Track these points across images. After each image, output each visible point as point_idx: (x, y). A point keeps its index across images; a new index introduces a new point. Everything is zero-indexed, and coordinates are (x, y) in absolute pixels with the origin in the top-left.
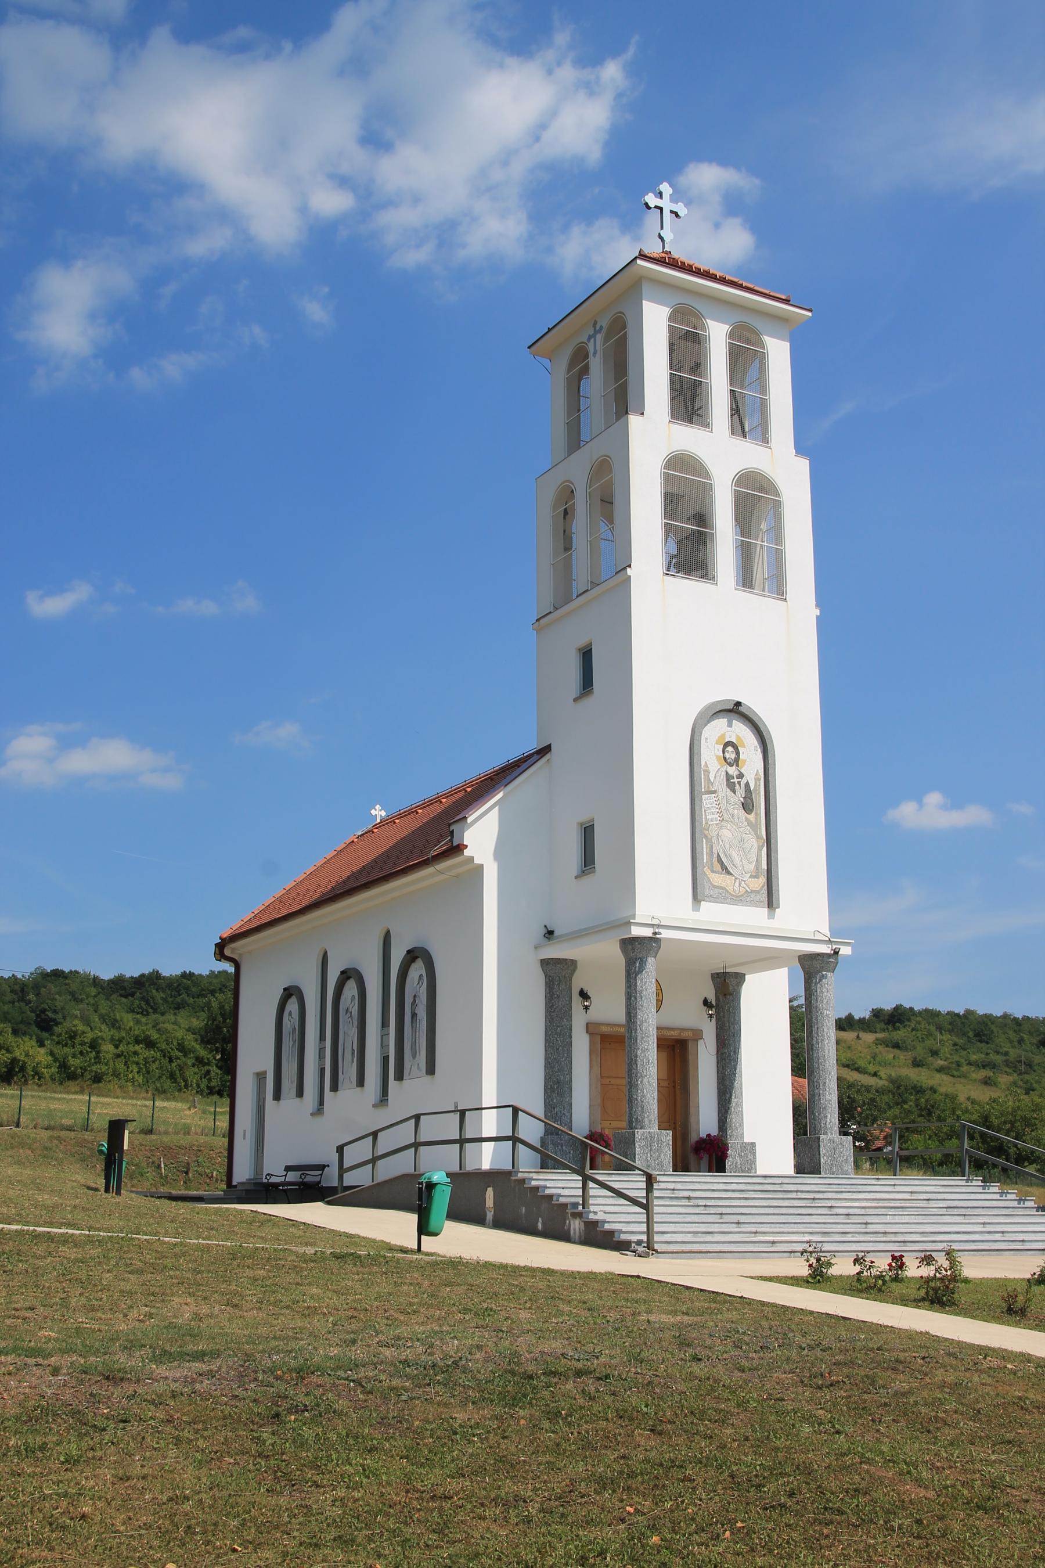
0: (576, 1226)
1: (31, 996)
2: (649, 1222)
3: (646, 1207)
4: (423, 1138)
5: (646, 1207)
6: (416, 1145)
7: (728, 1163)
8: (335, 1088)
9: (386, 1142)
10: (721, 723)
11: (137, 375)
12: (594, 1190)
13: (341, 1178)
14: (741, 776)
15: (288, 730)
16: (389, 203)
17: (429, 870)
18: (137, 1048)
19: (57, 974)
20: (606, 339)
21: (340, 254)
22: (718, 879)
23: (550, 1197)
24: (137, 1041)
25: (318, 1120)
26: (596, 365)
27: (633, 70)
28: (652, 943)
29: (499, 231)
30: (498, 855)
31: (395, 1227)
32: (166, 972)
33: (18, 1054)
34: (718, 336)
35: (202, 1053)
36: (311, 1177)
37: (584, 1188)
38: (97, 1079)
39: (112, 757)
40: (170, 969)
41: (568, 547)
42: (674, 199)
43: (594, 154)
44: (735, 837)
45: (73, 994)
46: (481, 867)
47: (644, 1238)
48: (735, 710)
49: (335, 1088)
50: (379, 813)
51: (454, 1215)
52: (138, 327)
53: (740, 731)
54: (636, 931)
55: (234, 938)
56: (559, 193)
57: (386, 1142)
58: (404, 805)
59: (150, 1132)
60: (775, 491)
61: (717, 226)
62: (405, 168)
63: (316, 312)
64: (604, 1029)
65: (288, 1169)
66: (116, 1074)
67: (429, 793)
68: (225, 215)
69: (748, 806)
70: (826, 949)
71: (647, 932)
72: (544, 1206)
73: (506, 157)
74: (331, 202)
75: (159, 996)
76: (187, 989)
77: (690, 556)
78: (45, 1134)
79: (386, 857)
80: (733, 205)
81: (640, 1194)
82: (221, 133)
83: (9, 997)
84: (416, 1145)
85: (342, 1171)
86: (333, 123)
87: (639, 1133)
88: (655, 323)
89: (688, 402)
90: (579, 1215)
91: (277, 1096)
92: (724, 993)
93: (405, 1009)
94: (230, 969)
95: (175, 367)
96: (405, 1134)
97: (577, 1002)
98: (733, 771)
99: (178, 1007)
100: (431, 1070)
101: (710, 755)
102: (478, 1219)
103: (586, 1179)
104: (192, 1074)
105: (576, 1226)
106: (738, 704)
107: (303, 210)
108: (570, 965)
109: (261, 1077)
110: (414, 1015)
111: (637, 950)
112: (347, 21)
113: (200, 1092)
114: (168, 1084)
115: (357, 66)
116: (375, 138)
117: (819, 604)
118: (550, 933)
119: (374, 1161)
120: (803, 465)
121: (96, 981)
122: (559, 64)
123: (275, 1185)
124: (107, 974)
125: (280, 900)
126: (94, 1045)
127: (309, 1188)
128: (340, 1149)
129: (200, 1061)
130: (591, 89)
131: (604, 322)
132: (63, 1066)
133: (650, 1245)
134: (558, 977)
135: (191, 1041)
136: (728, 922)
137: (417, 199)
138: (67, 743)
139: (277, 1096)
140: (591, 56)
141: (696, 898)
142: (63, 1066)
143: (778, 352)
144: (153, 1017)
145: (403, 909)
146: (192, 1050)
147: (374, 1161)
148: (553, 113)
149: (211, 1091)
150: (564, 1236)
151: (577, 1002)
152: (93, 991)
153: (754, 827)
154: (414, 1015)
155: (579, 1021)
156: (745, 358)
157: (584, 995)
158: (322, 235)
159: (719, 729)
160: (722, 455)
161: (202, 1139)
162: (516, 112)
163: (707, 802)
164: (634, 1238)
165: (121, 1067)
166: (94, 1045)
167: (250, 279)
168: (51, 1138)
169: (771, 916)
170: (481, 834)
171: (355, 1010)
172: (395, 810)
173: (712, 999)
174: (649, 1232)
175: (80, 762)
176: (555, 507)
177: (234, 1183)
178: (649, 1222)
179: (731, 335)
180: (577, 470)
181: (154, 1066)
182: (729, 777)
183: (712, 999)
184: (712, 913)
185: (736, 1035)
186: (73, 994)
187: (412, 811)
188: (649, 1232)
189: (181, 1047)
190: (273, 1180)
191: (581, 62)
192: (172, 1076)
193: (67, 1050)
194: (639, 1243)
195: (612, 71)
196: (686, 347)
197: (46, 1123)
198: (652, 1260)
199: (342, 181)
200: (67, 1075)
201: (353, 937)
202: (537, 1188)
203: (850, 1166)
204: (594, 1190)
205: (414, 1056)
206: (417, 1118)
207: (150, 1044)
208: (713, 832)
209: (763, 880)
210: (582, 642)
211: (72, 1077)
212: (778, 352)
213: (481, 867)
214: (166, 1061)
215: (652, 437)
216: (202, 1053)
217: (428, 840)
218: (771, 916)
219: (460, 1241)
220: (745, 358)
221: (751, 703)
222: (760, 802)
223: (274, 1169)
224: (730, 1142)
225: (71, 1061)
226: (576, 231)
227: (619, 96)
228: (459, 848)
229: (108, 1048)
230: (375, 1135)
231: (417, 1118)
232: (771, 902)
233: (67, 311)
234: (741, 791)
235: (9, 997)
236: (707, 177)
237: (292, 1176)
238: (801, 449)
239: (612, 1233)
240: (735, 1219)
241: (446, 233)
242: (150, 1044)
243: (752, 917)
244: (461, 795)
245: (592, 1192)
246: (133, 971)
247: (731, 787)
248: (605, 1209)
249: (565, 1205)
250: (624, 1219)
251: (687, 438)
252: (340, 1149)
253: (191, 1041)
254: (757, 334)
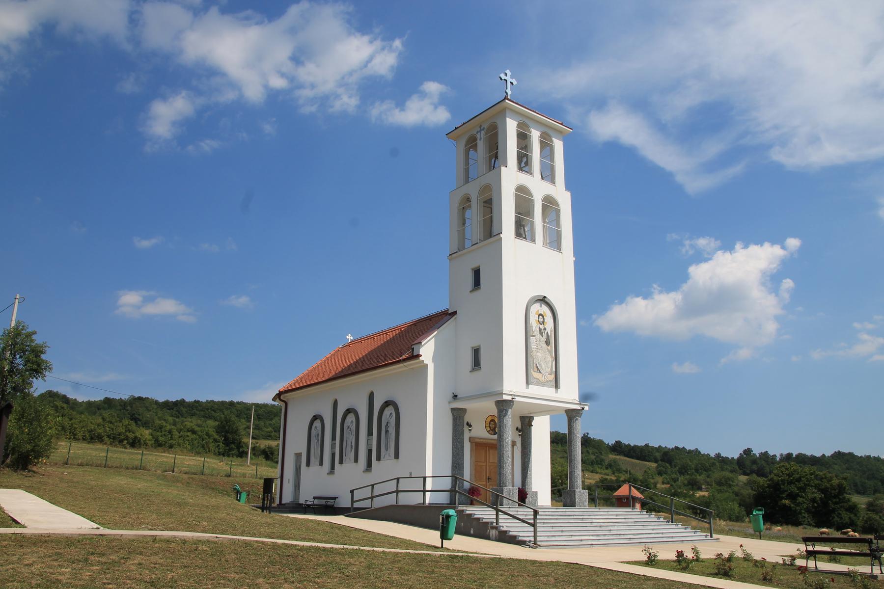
0: (493, 533)
1: (129, 408)
2: (535, 531)
3: (534, 525)
4: (400, 489)
5: (534, 525)
6: (397, 492)
7: (527, 500)
8: (341, 462)
9: (378, 490)
10: (538, 305)
11: (190, 148)
12: (501, 516)
13: (352, 504)
14: (545, 329)
15: (244, 300)
16: (301, 86)
17: (401, 365)
18: (189, 434)
19: (140, 398)
20: (486, 133)
21: (279, 104)
22: (536, 375)
23: (479, 519)
24: (188, 431)
25: (331, 476)
26: (481, 145)
27: (404, 44)
28: (510, 403)
29: (348, 102)
30: (434, 359)
31: (432, 537)
32: (187, 400)
33: (138, 434)
34: (535, 135)
35: (217, 437)
36: (330, 502)
37: (497, 515)
38: (171, 447)
39: (167, 306)
40: (189, 399)
41: (464, 224)
42: (512, 77)
43: (390, 77)
44: (543, 357)
45: (147, 408)
46: (427, 365)
47: (532, 539)
48: (543, 300)
49: (341, 462)
50: (350, 338)
51: (458, 532)
52: (192, 129)
53: (545, 309)
54: (505, 397)
55: (287, 391)
56: (371, 88)
57: (378, 490)
58: (364, 334)
59: (230, 476)
60: (558, 205)
61: (436, 107)
62: (309, 72)
63: (268, 128)
64: (477, 440)
65: (315, 498)
66: (179, 445)
67: (385, 327)
68: (234, 85)
69: (548, 343)
70: (578, 407)
71: (509, 398)
72: (474, 523)
73: (351, 73)
74: (278, 83)
75: (184, 410)
76: (196, 407)
77: (522, 230)
78: (186, 476)
79: (362, 360)
80: (443, 101)
81: (532, 521)
82: (234, 50)
83: (119, 408)
84: (397, 492)
85: (353, 502)
86: (282, 52)
87: (505, 489)
88: (511, 127)
89: (524, 162)
90: (496, 528)
91: (308, 464)
92: (525, 425)
93: (385, 428)
94: (283, 404)
95: (208, 145)
96: (392, 486)
97: (466, 428)
98: (542, 327)
99: (193, 415)
100: (397, 456)
101: (533, 319)
102: (468, 534)
103: (498, 511)
104: (212, 446)
105: (493, 533)
106: (545, 297)
107: (266, 86)
108: (464, 411)
109: (298, 456)
110: (387, 431)
111: (503, 406)
112: (294, 11)
113: (215, 454)
114: (201, 450)
115: (293, 31)
116: (297, 59)
117: (575, 255)
118: (456, 396)
119: (372, 498)
120: (568, 194)
121: (156, 402)
122: (375, 39)
123: (309, 506)
124: (161, 400)
125: (308, 375)
126: (170, 432)
127: (328, 507)
128: (352, 492)
129: (215, 440)
130: (391, 50)
131: (486, 126)
132: (157, 440)
133: (535, 542)
134: (458, 416)
135: (212, 431)
136: (541, 393)
137: (313, 86)
138: (147, 300)
139: (308, 464)
140: (388, 37)
141: (528, 383)
142: (157, 440)
143: (558, 146)
144: (181, 419)
145: (384, 383)
146: (212, 436)
147: (372, 498)
148: (371, 59)
149: (219, 454)
150: (487, 537)
151: (466, 428)
152: (155, 407)
153: (550, 352)
154: (387, 431)
155: (467, 435)
156: (546, 146)
157: (469, 425)
158: (273, 97)
159: (536, 308)
160: (539, 188)
161: (254, 480)
162: (352, 55)
163: (532, 340)
164: (528, 539)
165: (181, 441)
166: (170, 432)
167: (241, 112)
168: (189, 478)
169: (556, 392)
170: (427, 349)
171: (353, 427)
172: (358, 337)
173: (520, 427)
174: (535, 536)
175: (150, 309)
176: (460, 205)
177: (283, 502)
178: (535, 531)
179: (541, 136)
180: (473, 190)
181: (195, 442)
182: (540, 330)
183: (520, 427)
184: (535, 390)
185: (530, 444)
186: (147, 408)
187: (368, 338)
188: (535, 536)
189: (208, 434)
190: (308, 503)
191: (383, 40)
192: (203, 447)
193: (159, 434)
194: (530, 541)
195: (397, 43)
196: (523, 138)
197: (80, 461)
198: (538, 550)
199: (283, 75)
200: (158, 444)
201: (353, 394)
202: (471, 515)
203: (587, 503)
204: (501, 516)
205: (387, 450)
206: (398, 479)
207: (194, 432)
208: (534, 353)
209: (553, 376)
210: (475, 266)
211: (160, 445)
212: (558, 146)
213: (427, 365)
214: (200, 440)
215: (510, 177)
216: (217, 437)
217: (399, 348)
218: (556, 392)
219: (460, 543)
220: (546, 146)
221: (551, 298)
222: (553, 341)
223: (306, 497)
224: (528, 491)
225: (160, 438)
226: (377, 104)
227: (400, 54)
228: (418, 356)
229: (176, 434)
230: (373, 486)
231: (398, 479)
232: (557, 386)
233: (167, 114)
234: (545, 336)
235: (119, 408)
236: (433, 87)
237: (316, 502)
238: (568, 187)
239: (515, 537)
240: (561, 529)
241: (324, 100)
242: (194, 432)
243: (548, 392)
244: (399, 331)
245: (500, 517)
246: (173, 399)
247: (541, 334)
248: (507, 524)
249: (487, 523)
250: (524, 532)
251: (523, 179)
252: (352, 492)
253: (212, 431)
254: (550, 137)
